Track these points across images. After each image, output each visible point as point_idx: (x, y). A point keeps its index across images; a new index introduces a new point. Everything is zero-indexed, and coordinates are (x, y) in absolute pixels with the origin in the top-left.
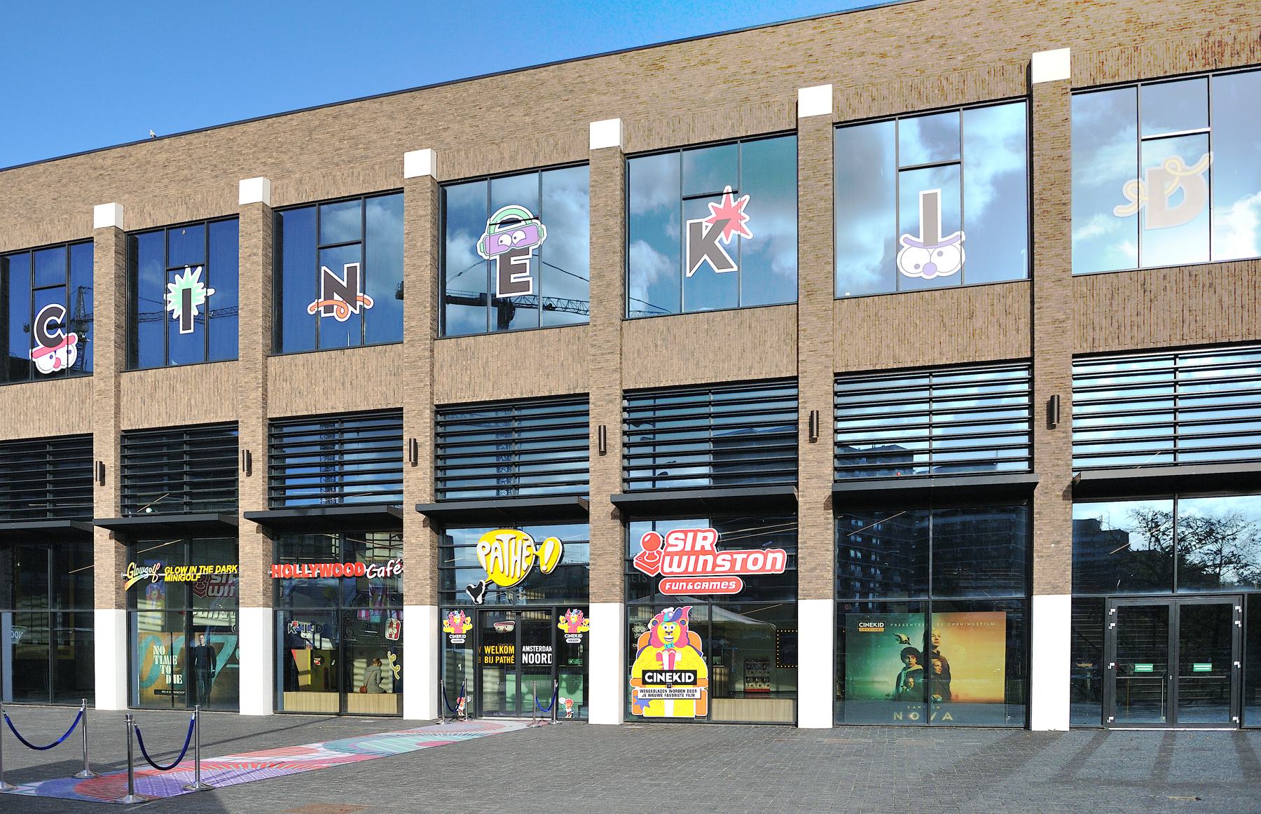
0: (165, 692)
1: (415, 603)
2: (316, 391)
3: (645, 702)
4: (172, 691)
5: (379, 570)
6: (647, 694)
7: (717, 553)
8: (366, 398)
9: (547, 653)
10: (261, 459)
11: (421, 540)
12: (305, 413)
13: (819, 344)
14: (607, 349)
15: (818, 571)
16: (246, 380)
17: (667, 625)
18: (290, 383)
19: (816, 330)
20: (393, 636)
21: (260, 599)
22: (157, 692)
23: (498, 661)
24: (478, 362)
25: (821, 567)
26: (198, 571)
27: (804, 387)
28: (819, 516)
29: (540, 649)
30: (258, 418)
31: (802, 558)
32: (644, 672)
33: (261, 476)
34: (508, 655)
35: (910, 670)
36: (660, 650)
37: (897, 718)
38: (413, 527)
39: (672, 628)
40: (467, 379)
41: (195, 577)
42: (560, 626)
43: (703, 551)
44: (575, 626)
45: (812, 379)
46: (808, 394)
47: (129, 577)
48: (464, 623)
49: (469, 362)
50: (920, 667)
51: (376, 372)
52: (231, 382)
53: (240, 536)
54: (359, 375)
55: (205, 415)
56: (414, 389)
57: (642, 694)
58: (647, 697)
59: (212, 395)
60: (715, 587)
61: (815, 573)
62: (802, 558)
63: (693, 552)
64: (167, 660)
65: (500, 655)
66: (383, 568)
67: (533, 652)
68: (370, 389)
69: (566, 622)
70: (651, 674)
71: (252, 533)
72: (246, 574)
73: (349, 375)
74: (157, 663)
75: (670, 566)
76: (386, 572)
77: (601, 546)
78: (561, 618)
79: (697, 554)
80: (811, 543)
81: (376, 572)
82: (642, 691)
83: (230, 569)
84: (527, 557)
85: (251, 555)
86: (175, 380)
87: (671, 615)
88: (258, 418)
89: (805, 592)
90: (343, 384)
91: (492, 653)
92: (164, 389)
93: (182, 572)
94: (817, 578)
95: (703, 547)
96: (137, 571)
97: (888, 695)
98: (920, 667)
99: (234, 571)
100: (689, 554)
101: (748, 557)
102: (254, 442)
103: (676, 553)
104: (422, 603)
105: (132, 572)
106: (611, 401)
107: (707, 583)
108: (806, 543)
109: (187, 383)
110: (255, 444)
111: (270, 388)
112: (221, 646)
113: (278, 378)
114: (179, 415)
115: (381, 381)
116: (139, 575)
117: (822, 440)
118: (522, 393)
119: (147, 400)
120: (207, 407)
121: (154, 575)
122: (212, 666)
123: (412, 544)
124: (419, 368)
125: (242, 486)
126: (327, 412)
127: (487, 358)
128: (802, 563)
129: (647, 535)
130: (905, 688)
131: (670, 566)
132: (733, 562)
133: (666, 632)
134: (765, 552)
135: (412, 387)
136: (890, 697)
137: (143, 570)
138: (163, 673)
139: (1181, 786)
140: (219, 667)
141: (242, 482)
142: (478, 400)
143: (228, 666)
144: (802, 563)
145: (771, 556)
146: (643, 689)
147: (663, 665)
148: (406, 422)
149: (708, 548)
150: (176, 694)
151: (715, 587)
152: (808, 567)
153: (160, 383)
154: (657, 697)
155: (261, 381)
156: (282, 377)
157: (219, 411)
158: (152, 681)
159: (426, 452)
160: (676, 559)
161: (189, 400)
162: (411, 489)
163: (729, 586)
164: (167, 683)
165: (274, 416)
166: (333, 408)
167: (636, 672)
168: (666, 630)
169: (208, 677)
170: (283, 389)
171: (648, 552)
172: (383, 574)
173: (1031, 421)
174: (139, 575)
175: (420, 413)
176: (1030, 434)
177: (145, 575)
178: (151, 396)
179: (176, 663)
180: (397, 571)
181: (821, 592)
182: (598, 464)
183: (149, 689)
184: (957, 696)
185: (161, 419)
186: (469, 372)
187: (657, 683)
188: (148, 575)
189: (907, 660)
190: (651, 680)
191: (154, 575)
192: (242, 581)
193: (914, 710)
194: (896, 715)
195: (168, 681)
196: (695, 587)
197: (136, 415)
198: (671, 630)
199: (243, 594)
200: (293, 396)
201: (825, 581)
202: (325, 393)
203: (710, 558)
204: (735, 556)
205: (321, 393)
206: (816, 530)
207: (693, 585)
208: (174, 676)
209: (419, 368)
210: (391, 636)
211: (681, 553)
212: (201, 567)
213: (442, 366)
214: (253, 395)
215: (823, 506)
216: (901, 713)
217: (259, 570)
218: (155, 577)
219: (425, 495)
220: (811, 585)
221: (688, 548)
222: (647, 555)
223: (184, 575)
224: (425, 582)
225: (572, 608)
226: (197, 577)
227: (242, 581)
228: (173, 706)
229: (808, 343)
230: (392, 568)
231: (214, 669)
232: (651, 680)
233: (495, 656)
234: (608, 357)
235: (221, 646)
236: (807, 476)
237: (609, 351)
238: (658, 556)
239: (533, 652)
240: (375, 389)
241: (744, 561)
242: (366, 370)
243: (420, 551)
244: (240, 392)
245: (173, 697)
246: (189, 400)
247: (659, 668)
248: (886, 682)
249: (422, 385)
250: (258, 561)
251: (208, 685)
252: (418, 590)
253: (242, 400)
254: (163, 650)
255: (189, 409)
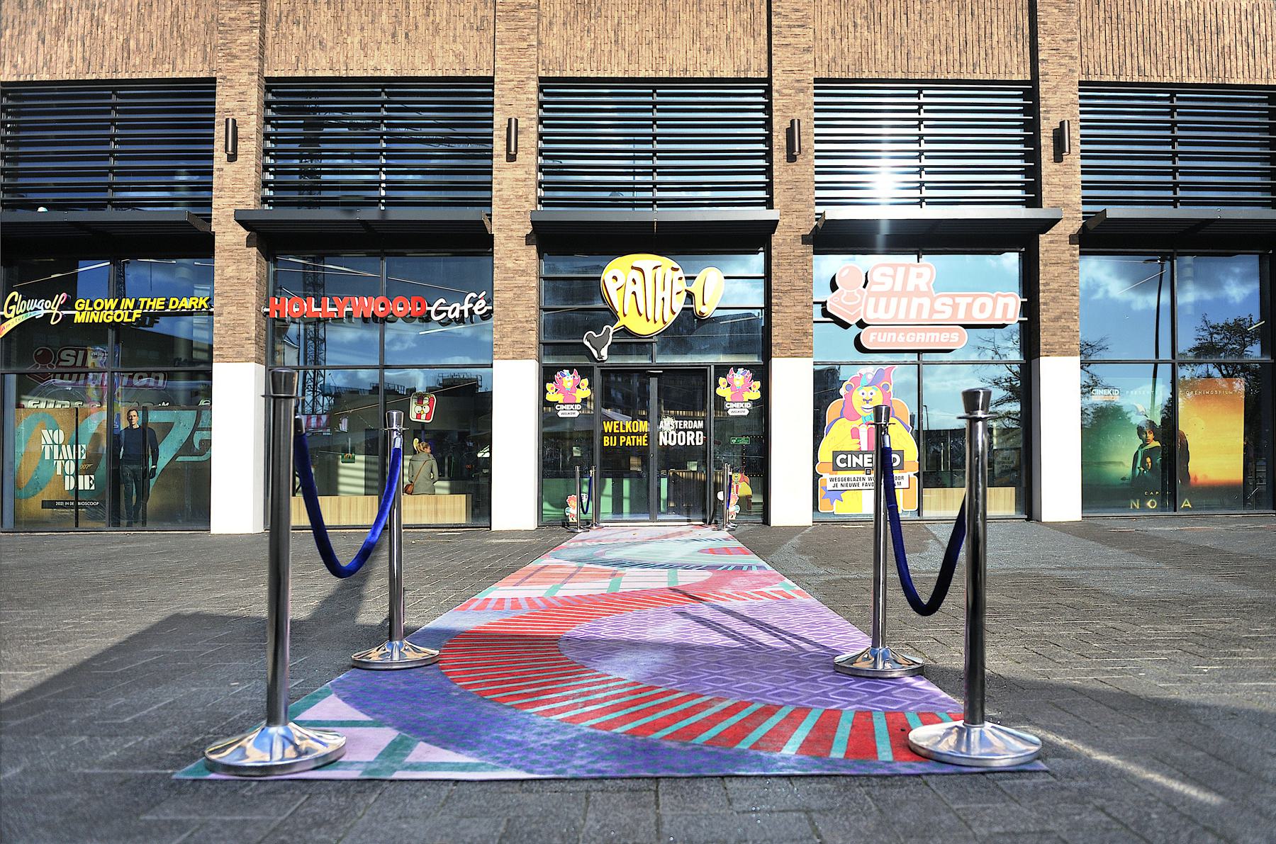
0: (62, 504)
1: (511, 356)
2: (349, 42)
3: (836, 494)
4: (77, 501)
5: (450, 309)
6: (839, 484)
7: (935, 296)
8: (432, 58)
9: (695, 430)
10: (254, 136)
11: (523, 264)
12: (329, 74)
13: (1061, 42)
14: (797, 20)
15: (1063, 320)
16: (233, 15)
17: (865, 390)
18: (305, 28)
19: (1058, 24)
20: (423, 417)
21: (252, 350)
22: (48, 504)
23: (624, 443)
24: (606, 23)
25: (1066, 316)
26: (136, 306)
27: (1046, 93)
28: (1064, 252)
29: (685, 425)
30: (252, 74)
31: (1045, 304)
32: (835, 454)
33: (253, 163)
34: (640, 434)
35: (1147, 447)
36: (856, 424)
37: (1134, 507)
38: (510, 245)
39: (863, 394)
40: (589, 45)
41: (130, 316)
42: (720, 392)
43: (917, 293)
44: (741, 391)
45: (1055, 84)
46: (1051, 102)
47: (7, 316)
48: (578, 387)
49: (593, 21)
50: (1158, 444)
51: (448, 22)
52: (201, 20)
53: (217, 250)
54: (420, 25)
55: (154, 66)
56: (512, 49)
57: (833, 483)
58: (840, 488)
59: (168, 36)
60: (932, 340)
61: (1060, 324)
62: (1045, 304)
63: (904, 293)
64: (68, 452)
65: (626, 435)
66: (457, 305)
67: (692, 430)
68: (438, 47)
69: (729, 385)
70: (845, 457)
71: (239, 247)
72: (226, 310)
73: (404, 24)
74: (47, 457)
75: (876, 311)
76: (462, 312)
77: (788, 280)
78: (721, 380)
79: (910, 295)
80: (1054, 285)
81: (447, 311)
82: (831, 480)
83: (195, 304)
84: (678, 293)
85: (236, 281)
86: (103, 9)
87: (870, 377)
88: (252, 74)
89: (1048, 347)
90: (394, 35)
91: (615, 431)
92: (81, 22)
93: (107, 308)
94: (1064, 329)
95: (917, 287)
96: (22, 305)
97: (1123, 479)
98: (1158, 444)
99: (203, 307)
100: (900, 295)
101: (973, 301)
102: (243, 110)
103: (883, 294)
104: (522, 356)
105: (13, 307)
106: (802, 91)
107: (923, 334)
108: (1049, 285)
109: (124, 16)
110: (245, 113)
111: (270, 32)
112: (167, 427)
113: (284, 19)
114: (106, 64)
115: (455, 36)
116: (26, 312)
117: (1069, 160)
118: (671, 71)
119: (48, 37)
120: (158, 53)
121: (55, 311)
122: (150, 459)
123: (507, 270)
124: (521, 20)
125: (220, 177)
126: (365, 75)
127: (620, 18)
128: (1044, 310)
129: (844, 269)
130: (1142, 469)
131: (876, 311)
132: (955, 307)
133: (864, 400)
134: (994, 295)
135: (508, 47)
136: (1126, 481)
137: (33, 304)
138: (59, 472)
139: (1070, 775)
140: (163, 461)
141: (219, 170)
142: (606, 76)
143: (180, 459)
144: (1044, 310)
145: (1001, 301)
146: (834, 476)
147: (859, 443)
148: (498, 97)
149: (924, 288)
150: (82, 507)
151: (932, 340)
152: (1052, 315)
153: (75, 12)
154: (852, 488)
155: (257, 18)
156: (290, 18)
157: (179, 61)
158: (37, 486)
159: (529, 142)
160: (883, 301)
161: (127, 40)
162: (505, 194)
163: (950, 339)
164: (67, 488)
165: (276, 75)
166: (376, 69)
167: (825, 455)
168: (864, 397)
169: (144, 477)
170: (292, 34)
171: (845, 291)
172: (457, 314)
173: (768, 155)
174: (26, 312)
175: (521, 85)
176: (768, 171)
177: (38, 312)
178: (57, 32)
179: (84, 457)
180: (479, 310)
181: (1067, 347)
182: (785, 174)
183: (31, 500)
184: (1196, 478)
185: (74, 68)
186: (593, 35)
187: (852, 469)
188: (42, 313)
189: (1144, 436)
190: (845, 465)
191: (55, 311)
192: (219, 322)
193: (1151, 497)
194: (1132, 502)
195: (69, 484)
196: (908, 340)
197: (27, 58)
198: (871, 397)
199: (220, 342)
200: (309, 47)
201: (1071, 333)
202: (363, 47)
203: (926, 302)
204: (958, 300)
205: (357, 46)
206: (1061, 269)
207: (905, 336)
208: (80, 477)
209: (521, 20)
210: (419, 416)
211: (890, 294)
212: (143, 300)
213: (551, 23)
214: (245, 38)
215: (1068, 239)
216: (1138, 501)
217: (249, 305)
218: (57, 315)
219: (527, 205)
220: (1056, 339)
221: (898, 288)
222: (845, 295)
223: (111, 312)
224: (528, 326)
225: (736, 367)
226: (135, 316)
227: (219, 322)
228: (77, 526)
229: (1048, 39)
230: (471, 305)
231: (155, 463)
232: (845, 465)
233: (619, 435)
234: (797, 31)
235: (167, 427)
236: (1052, 203)
237: (800, 24)
238: (859, 296)
239: (692, 430)
240: (447, 47)
241: (969, 306)
242: (431, 18)
243: (521, 280)
244: (220, 32)
245: (77, 511)
246: (127, 40)
247: (855, 448)
248: (1121, 463)
249: (525, 45)
250: (248, 291)
251: (143, 494)
252: (517, 336)
253: (224, 44)
254: (60, 436)
255: (125, 55)
